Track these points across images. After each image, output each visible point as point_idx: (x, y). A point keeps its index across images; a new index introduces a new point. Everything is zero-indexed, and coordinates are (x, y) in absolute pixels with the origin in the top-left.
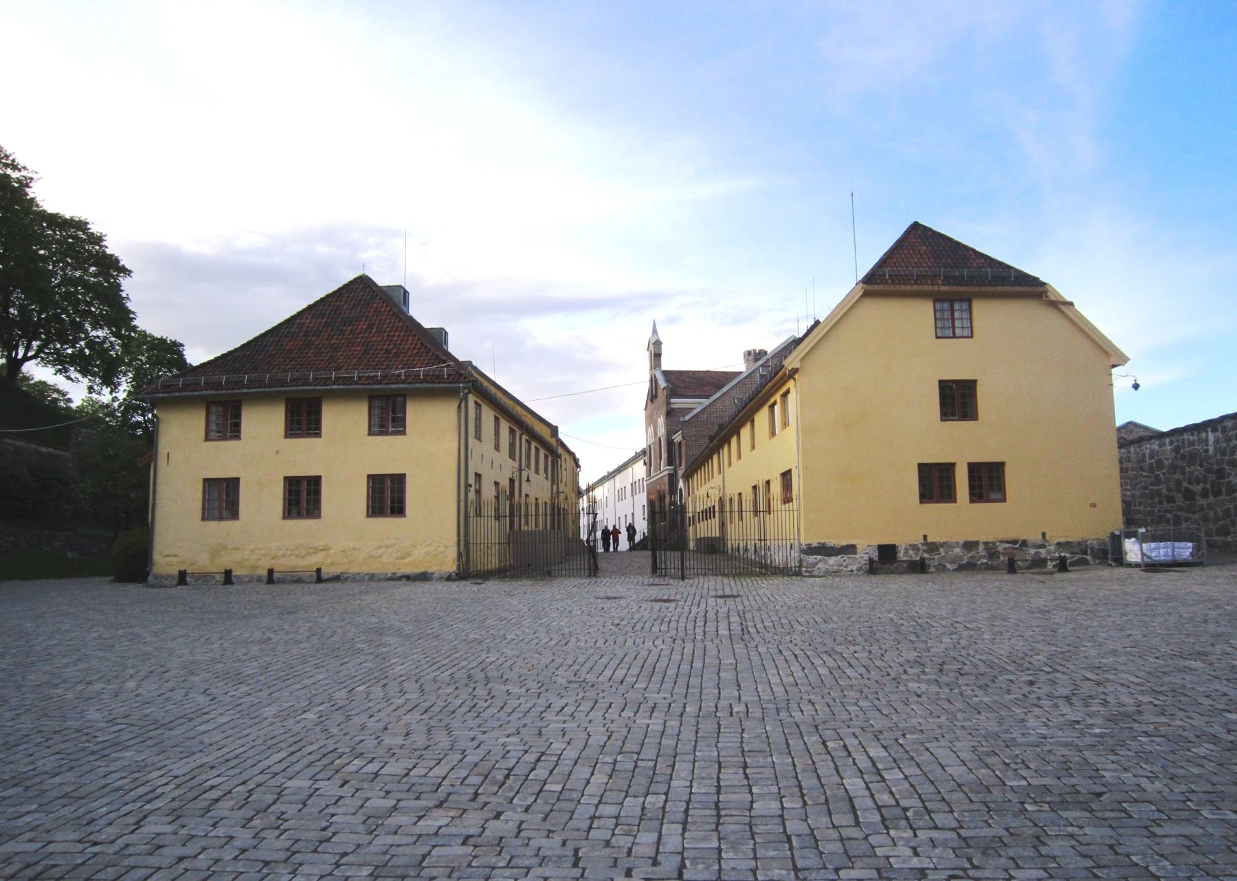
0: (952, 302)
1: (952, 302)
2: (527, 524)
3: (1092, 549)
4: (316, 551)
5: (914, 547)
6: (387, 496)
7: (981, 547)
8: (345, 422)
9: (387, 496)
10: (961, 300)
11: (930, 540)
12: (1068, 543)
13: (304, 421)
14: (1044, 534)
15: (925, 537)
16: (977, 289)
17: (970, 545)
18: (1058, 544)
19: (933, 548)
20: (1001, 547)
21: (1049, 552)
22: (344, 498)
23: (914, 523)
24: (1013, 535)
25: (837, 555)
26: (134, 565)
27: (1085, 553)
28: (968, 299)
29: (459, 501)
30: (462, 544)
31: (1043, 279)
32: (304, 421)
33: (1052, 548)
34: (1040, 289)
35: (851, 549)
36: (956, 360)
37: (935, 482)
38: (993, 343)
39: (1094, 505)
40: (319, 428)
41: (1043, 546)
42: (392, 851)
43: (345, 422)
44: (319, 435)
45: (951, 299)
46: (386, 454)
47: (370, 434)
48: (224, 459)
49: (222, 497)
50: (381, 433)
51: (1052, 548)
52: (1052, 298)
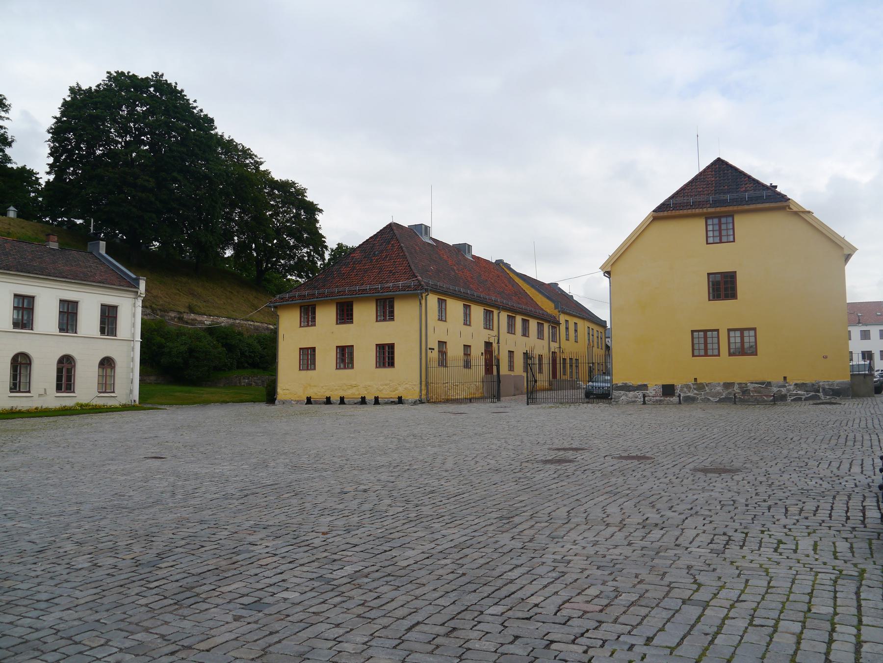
0: (720, 218)
1: (720, 218)
2: (564, 374)
3: (824, 389)
4: (353, 386)
5: (688, 387)
6: (386, 355)
7: (736, 386)
8: (365, 313)
9: (386, 355)
10: (727, 216)
11: (699, 382)
12: (803, 384)
13: (345, 315)
14: (785, 378)
15: (696, 379)
16: (735, 208)
17: (728, 385)
18: (796, 384)
19: (700, 387)
20: (751, 387)
21: (789, 390)
22: (365, 357)
23: (685, 370)
24: (760, 378)
25: (634, 391)
26: (271, 397)
27: (818, 392)
28: (731, 215)
29: (421, 359)
30: (424, 383)
31: (789, 196)
32: (345, 315)
33: (792, 387)
34: (785, 204)
35: (644, 387)
36: (722, 258)
37: (703, 342)
38: (752, 241)
39: (825, 357)
40: (341, 323)
41: (784, 386)
42: (430, 648)
43: (365, 313)
44: (352, 322)
45: (719, 216)
46: (385, 333)
47: (377, 321)
48: (308, 337)
49: (308, 357)
50: (385, 320)
51: (792, 387)
52: (795, 209)
